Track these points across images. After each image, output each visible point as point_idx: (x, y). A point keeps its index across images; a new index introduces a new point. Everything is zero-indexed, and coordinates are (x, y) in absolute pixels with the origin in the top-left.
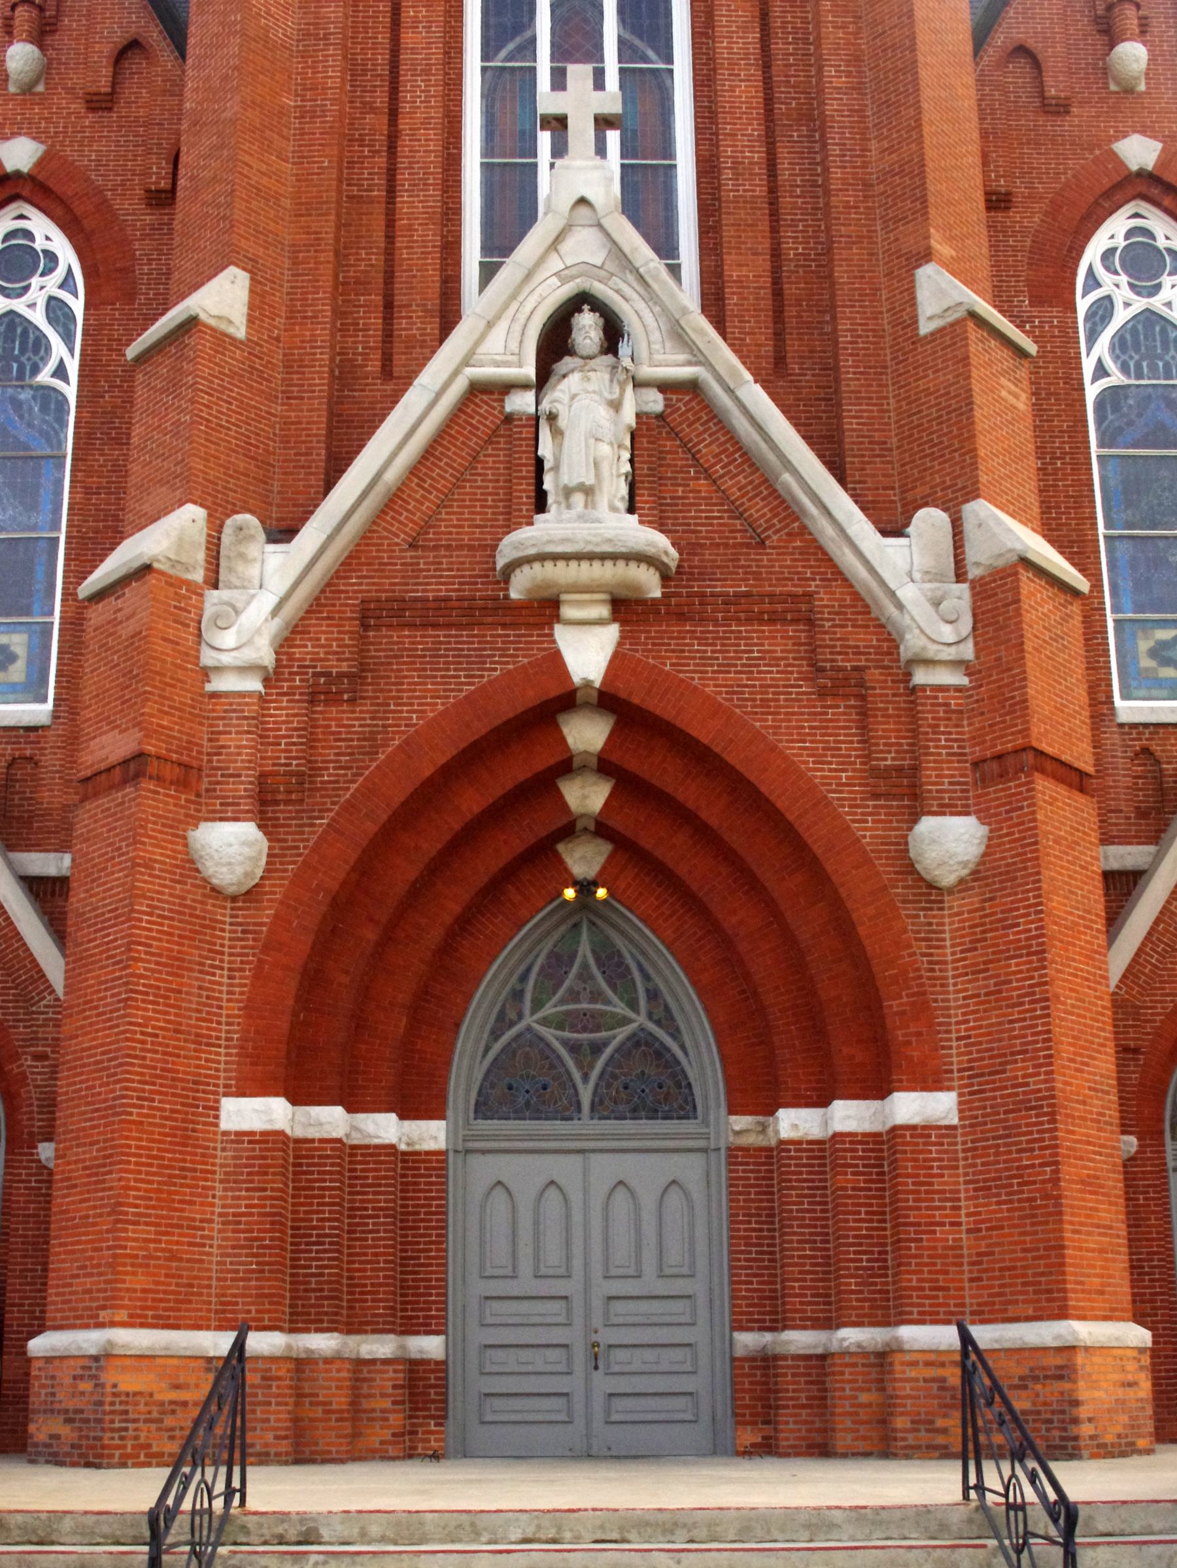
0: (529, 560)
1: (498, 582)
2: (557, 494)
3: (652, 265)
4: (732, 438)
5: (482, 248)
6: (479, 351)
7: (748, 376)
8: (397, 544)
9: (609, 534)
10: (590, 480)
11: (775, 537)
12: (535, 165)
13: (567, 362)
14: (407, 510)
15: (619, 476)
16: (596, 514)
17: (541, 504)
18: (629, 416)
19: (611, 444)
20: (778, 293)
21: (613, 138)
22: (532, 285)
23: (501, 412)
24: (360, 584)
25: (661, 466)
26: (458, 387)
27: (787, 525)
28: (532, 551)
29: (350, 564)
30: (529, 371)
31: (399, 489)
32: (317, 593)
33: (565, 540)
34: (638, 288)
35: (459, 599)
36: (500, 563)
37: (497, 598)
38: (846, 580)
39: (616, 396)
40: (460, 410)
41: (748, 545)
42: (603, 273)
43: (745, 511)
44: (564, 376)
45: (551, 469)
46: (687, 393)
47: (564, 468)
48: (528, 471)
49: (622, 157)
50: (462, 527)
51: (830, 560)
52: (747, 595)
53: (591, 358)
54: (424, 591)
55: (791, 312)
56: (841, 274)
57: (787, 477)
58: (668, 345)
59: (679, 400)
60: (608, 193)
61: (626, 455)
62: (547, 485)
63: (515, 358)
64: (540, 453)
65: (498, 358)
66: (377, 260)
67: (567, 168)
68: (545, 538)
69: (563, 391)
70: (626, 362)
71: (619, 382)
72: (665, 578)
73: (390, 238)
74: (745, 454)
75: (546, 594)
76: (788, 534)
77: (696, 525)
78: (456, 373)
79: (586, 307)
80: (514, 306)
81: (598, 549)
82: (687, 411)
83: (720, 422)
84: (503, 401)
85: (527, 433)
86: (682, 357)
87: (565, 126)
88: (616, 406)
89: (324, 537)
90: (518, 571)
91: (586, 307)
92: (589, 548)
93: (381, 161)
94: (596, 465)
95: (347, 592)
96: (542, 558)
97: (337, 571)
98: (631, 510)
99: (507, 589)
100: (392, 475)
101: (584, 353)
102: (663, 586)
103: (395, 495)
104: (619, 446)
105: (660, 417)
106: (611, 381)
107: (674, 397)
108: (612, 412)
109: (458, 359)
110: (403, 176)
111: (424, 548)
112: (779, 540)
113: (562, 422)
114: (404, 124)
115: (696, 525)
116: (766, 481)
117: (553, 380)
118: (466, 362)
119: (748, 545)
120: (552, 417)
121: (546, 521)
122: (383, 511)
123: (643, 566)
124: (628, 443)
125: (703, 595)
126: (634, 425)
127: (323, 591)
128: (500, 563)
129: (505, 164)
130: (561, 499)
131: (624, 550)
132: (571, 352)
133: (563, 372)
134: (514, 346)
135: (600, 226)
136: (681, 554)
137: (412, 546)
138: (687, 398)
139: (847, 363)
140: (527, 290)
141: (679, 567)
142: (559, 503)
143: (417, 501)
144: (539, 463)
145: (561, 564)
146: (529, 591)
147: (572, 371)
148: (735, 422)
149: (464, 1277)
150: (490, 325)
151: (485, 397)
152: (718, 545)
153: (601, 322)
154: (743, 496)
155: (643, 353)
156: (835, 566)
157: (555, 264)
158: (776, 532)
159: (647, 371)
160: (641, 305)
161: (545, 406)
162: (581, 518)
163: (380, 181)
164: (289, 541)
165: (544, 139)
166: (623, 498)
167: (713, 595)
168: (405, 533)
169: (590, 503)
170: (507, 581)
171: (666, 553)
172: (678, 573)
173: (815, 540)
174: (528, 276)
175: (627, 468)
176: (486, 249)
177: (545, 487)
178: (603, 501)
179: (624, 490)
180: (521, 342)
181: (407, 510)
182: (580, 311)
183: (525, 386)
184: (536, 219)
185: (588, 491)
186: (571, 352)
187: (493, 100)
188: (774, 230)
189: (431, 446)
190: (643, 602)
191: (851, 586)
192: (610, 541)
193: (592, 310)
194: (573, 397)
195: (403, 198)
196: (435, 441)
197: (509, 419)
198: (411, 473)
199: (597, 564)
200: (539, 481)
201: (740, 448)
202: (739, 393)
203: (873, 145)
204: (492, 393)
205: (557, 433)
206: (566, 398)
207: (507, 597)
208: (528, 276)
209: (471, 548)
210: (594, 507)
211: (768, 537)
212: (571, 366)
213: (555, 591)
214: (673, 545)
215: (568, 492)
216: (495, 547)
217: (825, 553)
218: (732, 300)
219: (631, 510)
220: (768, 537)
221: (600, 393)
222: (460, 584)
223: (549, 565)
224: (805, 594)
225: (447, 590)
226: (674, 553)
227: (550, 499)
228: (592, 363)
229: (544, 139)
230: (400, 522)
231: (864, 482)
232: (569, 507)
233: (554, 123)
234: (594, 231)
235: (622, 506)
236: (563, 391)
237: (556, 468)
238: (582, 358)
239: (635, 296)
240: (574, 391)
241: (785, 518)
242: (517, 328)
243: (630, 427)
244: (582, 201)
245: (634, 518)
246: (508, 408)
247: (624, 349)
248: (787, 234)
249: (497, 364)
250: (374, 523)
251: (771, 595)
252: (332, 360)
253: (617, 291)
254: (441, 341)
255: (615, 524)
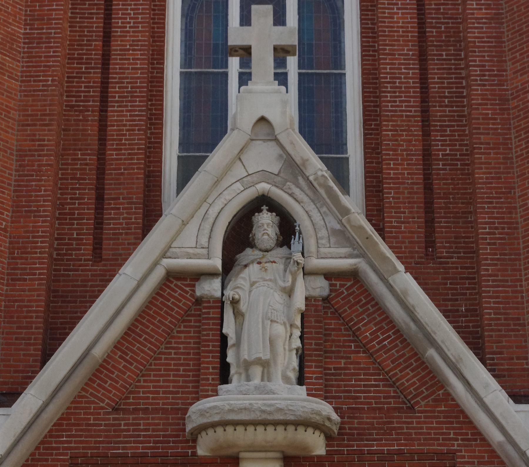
0: (214, 425)
1: (187, 441)
2: (238, 366)
3: (320, 173)
4: (387, 317)
5: (180, 144)
6: (174, 245)
7: (401, 267)
8: (102, 408)
9: (282, 404)
10: (265, 355)
11: (423, 403)
12: (226, 75)
13: (249, 254)
14: (111, 379)
15: (290, 350)
16: (270, 385)
17: (225, 378)
18: (299, 302)
19: (284, 324)
20: (428, 187)
21: (292, 62)
22: (220, 189)
23: (192, 296)
24: (70, 442)
25: (326, 341)
26: (159, 274)
27: (433, 393)
28: (217, 418)
29: (62, 425)
30: (217, 263)
31: (105, 361)
32: (32, 450)
33: (241, 410)
34: (308, 192)
35: (154, 455)
36: (189, 427)
37: (186, 455)
38: (484, 439)
39: (289, 284)
40: (158, 294)
41: (399, 410)
42: (278, 179)
43: (398, 380)
44: (246, 266)
45: (234, 345)
46: (350, 280)
47: (244, 346)
48: (214, 346)
49: (299, 68)
50: (158, 393)
51: (471, 422)
52: (400, 453)
53: (267, 251)
54: (124, 448)
55: (439, 203)
56: (480, 175)
57: (432, 352)
58: (333, 240)
59: (342, 286)
60: (284, 113)
61: (297, 333)
62: (230, 358)
63: (205, 251)
64: (224, 331)
65: (191, 251)
66: (91, 159)
67: (250, 92)
68: (227, 407)
69: (244, 279)
70: (298, 256)
71: (291, 272)
72: (329, 438)
73: (102, 140)
74: (398, 331)
75: (230, 452)
76: (434, 400)
77: (356, 392)
78: (156, 264)
79: (265, 208)
80: (205, 206)
81: (270, 418)
82: (349, 295)
83: (377, 304)
84: (194, 286)
85: (214, 313)
86: (344, 251)
87: (250, 54)
88: (289, 292)
89: (40, 403)
90: (203, 434)
91: (265, 208)
92: (264, 416)
93: (96, 75)
94: (272, 342)
95: (58, 449)
96: (224, 424)
97: (51, 431)
98: (300, 381)
99: (195, 447)
100: (99, 351)
101: (263, 247)
102: (327, 446)
103: (101, 366)
104: (291, 326)
105: (326, 299)
106: (285, 271)
107: (338, 283)
108: (285, 297)
109: (157, 253)
110: (114, 89)
111: (125, 411)
112: (426, 406)
113: (243, 307)
114: (116, 45)
115: (356, 392)
116: (416, 354)
117: (236, 269)
118: (164, 255)
119: (399, 410)
120: (235, 302)
121: (228, 391)
122: (90, 379)
123: (310, 430)
124: (298, 323)
125: (361, 452)
126: (303, 308)
127: (37, 448)
128: (189, 427)
129: (200, 73)
130: (242, 370)
131: (292, 418)
132: (252, 245)
133: (245, 263)
134: (204, 241)
135: (276, 140)
136: (341, 417)
137: (116, 410)
138: (349, 284)
139: (485, 250)
140: (215, 194)
141: (340, 428)
142: (240, 374)
143: (120, 371)
144: (224, 339)
145: (240, 429)
146: (212, 450)
147: (252, 262)
148: (388, 305)
149: (171, 144)
150: (184, 224)
151: (179, 283)
152: (374, 409)
153: (277, 219)
154: (395, 368)
155: (311, 245)
156: (475, 428)
157: (239, 171)
158: (423, 399)
159: (315, 263)
160: (311, 207)
161: (229, 293)
162: (258, 389)
163: (95, 93)
164: (9, 405)
165: (234, 63)
166: (294, 369)
167: (369, 452)
168: (109, 398)
169: (267, 376)
170: (195, 441)
171: (329, 419)
172: (339, 434)
173: (457, 405)
174: (217, 183)
175: (297, 343)
176: (184, 144)
177: (228, 360)
178: (278, 372)
179: (295, 363)
180: (210, 237)
181: (111, 379)
182: (260, 211)
183: (211, 274)
184: (226, 132)
185: (265, 365)
186: (252, 245)
187: (192, 19)
188: (426, 134)
189: (133, 324)
190: (310, 459)
191: (489, 445)
192: (280, 410)
193: (268, 210)
194: (252, 284)
195: (113, 108)
196: (136, 320)
197: (199, 301)
198: (115, 347)
199: (270, 429)
200: (224, 355)
201: (394, 326)
202: (390, 280)
203: (509, 65)
204: (185, 279)
205: (238, 314)
206: (247, 286)
207: (194, 454)
208: (217, 183)
209: (165, 411)
210: (269, 380)
211: (418, 403)
212: (252, 258)
213: (235, 450)
214: (336, 409)
215: (247, 365)
216: (186, 410)
217: (466, 417)
218: (390, 196)
219: (300, 381)
220: (418, 403)
221: (275, 281)
222: (155, 442)
223: (230, 429)
224: (449, 452)
225: (143, 448)
226: (335, 417)
227: (233, 370)
228: (270, 256)
229: (234, 63)
230: (104, 388)
231: (501, 353)
232: (248, 379)
233: (241, 52)
234: (273, 143)
235: (293, 376)
236: (244, 279)
237: (238, 344)
238: (261, 250)
239: (306, 199)
240: (253, 280)
241: (432, 386)
242: (207, 226)
243: (299, 310)
244: (263, 119)
245: (302, 391)
246: (198, 293)
247: (296, 245)
248: (436, 136)
249: (190, 256)
250: (83, 389)
251: (420, 453)
252: (51, 246)
253: (291, 195)
254: (144, 236)
255: (285, 396)
